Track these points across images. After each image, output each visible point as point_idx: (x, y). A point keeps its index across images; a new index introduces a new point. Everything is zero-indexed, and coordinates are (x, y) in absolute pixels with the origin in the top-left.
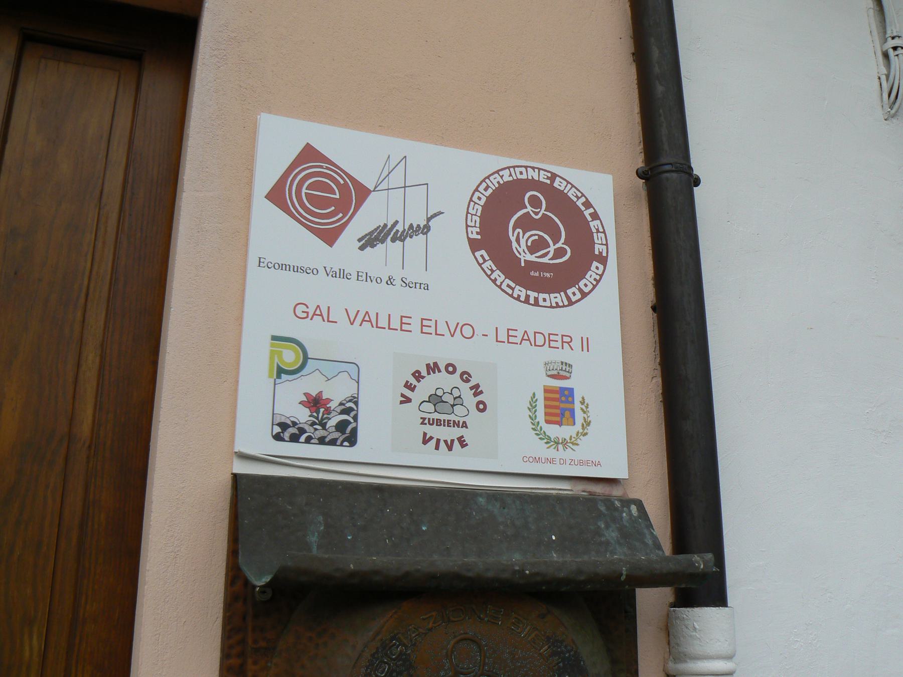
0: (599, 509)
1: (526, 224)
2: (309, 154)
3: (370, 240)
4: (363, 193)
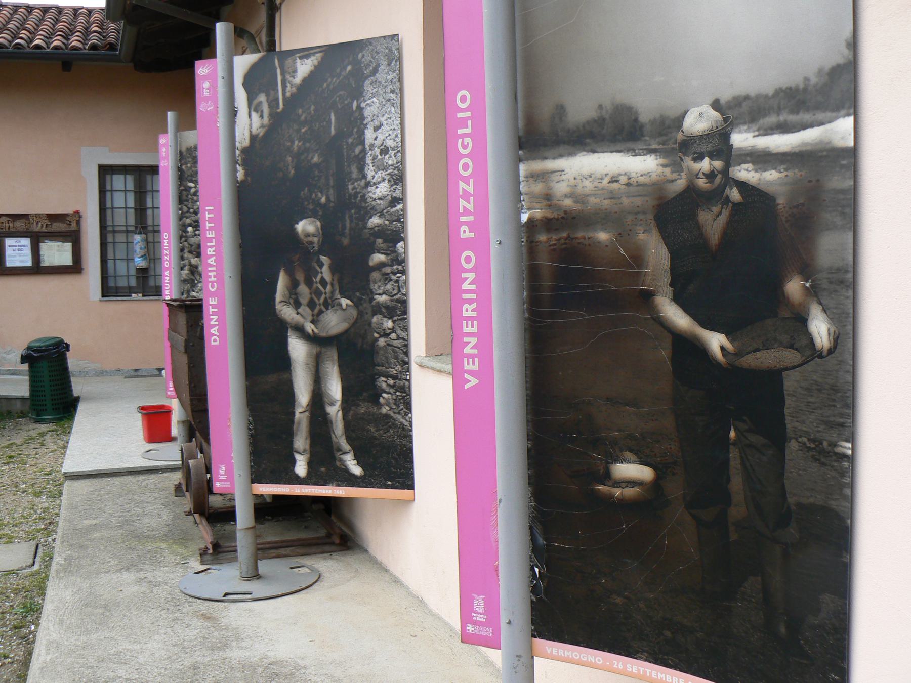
0: (305, 80)
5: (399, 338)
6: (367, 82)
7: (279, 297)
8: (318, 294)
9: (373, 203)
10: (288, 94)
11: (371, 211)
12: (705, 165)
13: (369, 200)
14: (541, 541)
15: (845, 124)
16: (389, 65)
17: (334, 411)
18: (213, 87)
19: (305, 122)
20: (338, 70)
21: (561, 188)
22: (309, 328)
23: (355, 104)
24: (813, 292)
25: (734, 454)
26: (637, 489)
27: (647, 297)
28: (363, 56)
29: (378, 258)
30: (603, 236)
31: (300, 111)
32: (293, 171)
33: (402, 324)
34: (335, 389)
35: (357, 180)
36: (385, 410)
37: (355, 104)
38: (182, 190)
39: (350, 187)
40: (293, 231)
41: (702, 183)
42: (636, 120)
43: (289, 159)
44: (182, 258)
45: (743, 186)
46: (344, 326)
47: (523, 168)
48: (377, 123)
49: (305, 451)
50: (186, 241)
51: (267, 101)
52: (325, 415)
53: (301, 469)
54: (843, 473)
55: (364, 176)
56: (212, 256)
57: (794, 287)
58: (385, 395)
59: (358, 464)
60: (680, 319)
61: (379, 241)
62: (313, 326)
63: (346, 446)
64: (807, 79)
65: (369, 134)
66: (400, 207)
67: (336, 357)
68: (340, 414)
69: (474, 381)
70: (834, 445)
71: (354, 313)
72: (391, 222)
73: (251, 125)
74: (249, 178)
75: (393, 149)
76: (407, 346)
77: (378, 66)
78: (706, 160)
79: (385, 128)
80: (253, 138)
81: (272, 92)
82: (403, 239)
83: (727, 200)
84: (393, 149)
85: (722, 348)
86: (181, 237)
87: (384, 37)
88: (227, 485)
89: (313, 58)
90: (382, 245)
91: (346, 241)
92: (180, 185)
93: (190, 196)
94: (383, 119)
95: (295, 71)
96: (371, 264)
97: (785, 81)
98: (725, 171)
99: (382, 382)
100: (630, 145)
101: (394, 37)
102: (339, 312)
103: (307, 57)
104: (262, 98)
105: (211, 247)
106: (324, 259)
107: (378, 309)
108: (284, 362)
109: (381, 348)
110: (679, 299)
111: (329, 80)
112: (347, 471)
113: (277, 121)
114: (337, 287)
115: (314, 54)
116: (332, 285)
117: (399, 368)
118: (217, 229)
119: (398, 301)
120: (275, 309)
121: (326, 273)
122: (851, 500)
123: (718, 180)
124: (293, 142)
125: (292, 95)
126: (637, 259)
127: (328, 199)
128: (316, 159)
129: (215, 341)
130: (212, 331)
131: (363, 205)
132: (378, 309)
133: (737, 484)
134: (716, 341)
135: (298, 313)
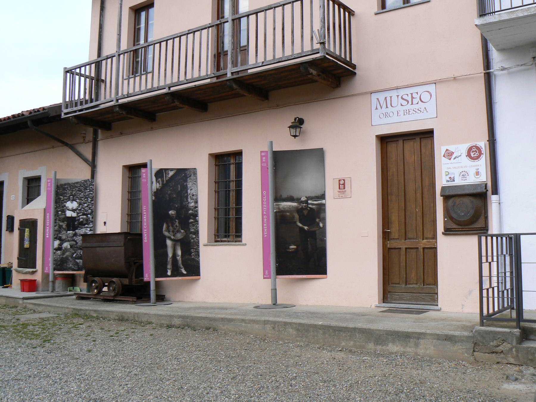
0: (171, 176)
1: (473, 152)
2: (447, 150)
3: (455, 159)
4: (453, 153)
5: (197, 240)
6: (188, 179)
7: (164, 230)
8: (175, 229)
9: (190, 207)
10: (167, 179)
11: (190, 209)
12: (304, 205)
13: (189, 207)
14: (278, 260)
15: (324, 201)
16: (194, 175)
17: (179, 258)
18: (147, 175)
19: (171, 187)
20: (180, 175)
21: (281, 207)
22: (172, 237)
23: (185, 183)
24: (320, 221)
25: (309, 243)
26: (294, 249)
27: (295, 222)
28: (187, 172)
29: (191, 220)
30: (288, 214)
31: (170, 184)
32: (168, 199)
33: (197, 236)
34: (179, 252)
35: (186, 202)
37: (185, 183)
38: (57, 199)
39: (184, 203)
40: (168, 214)
41: (304, 207)
42: (294, 198)
43: (167, 195)
44: (55, 223)
45: (310, 207)
46: (182, 237)
47: (275, 204)
48: (191, 189)
49: (170, 268)
50: (58, 217)
51: (161, 180)
53: (169, 273)
54: (325, 242)
55: (188, 201)
56: (145, 219)
57: (317, 220)
58: (193, 253)
59: (185, 271)
60: (300, 225)
61: (192, 216)
62: (173, 237)
63: (182, 266)
64: (319, 195)
65: (189, 191)
66: (197, 209)
67: (180, 244)
68: (181, 258)
69: (266, 236)
70: (323, 239)
71: (185, 234)
72: (195, 212)
73: (157, 186)
74: (156, 200)
75: (195, 195)
76: (199, 241)
77: (191, 175)
78: (304, 204)
80: (157, 189)
81: (163, 178)
82: (198, 216)
83: (308, 209)
84: (195, 195)
85: (307, 228)
86: (55, 215)
87: (193, 168)
88: (148, 279)
89: (174, 171)
90: (192, 218)
91: (183, 216)
92: (56, 197)
93: (60, 201)
94: (192, 188)
95: (169, 174)
96: (190, 222)
98: (307, 206)
99: (192, 250)
100: (293, 201)
101: (195, 169)
102: (181, 234)
103: (172, 171)
104: (160, 179)
105: (145, 216)
106: (177, 220)
107: (191, 233)
108: (165, 246)
109: (192, 242)
110: (300, 222)
111: (178, 177)
113: (164, 186)
114: (180, 227)
115: (174, 170)
116: (179, 227)
117: (197, 247)
118: (147, 212)
119: (196, 231)
120: (163, 233)
121: (177, 224)
122: (326, 245)
123: (306, 207)
124: (168, 191)
125: (168, 180)
126: (294, 217)
127: (178, 206)
128: (175, 196)
129: (146, 241)
130: (145, 238)
131: (187, 208)
132: (191, 233)
133: (309, 246)
134: (306, 228)
135: (169, 234)
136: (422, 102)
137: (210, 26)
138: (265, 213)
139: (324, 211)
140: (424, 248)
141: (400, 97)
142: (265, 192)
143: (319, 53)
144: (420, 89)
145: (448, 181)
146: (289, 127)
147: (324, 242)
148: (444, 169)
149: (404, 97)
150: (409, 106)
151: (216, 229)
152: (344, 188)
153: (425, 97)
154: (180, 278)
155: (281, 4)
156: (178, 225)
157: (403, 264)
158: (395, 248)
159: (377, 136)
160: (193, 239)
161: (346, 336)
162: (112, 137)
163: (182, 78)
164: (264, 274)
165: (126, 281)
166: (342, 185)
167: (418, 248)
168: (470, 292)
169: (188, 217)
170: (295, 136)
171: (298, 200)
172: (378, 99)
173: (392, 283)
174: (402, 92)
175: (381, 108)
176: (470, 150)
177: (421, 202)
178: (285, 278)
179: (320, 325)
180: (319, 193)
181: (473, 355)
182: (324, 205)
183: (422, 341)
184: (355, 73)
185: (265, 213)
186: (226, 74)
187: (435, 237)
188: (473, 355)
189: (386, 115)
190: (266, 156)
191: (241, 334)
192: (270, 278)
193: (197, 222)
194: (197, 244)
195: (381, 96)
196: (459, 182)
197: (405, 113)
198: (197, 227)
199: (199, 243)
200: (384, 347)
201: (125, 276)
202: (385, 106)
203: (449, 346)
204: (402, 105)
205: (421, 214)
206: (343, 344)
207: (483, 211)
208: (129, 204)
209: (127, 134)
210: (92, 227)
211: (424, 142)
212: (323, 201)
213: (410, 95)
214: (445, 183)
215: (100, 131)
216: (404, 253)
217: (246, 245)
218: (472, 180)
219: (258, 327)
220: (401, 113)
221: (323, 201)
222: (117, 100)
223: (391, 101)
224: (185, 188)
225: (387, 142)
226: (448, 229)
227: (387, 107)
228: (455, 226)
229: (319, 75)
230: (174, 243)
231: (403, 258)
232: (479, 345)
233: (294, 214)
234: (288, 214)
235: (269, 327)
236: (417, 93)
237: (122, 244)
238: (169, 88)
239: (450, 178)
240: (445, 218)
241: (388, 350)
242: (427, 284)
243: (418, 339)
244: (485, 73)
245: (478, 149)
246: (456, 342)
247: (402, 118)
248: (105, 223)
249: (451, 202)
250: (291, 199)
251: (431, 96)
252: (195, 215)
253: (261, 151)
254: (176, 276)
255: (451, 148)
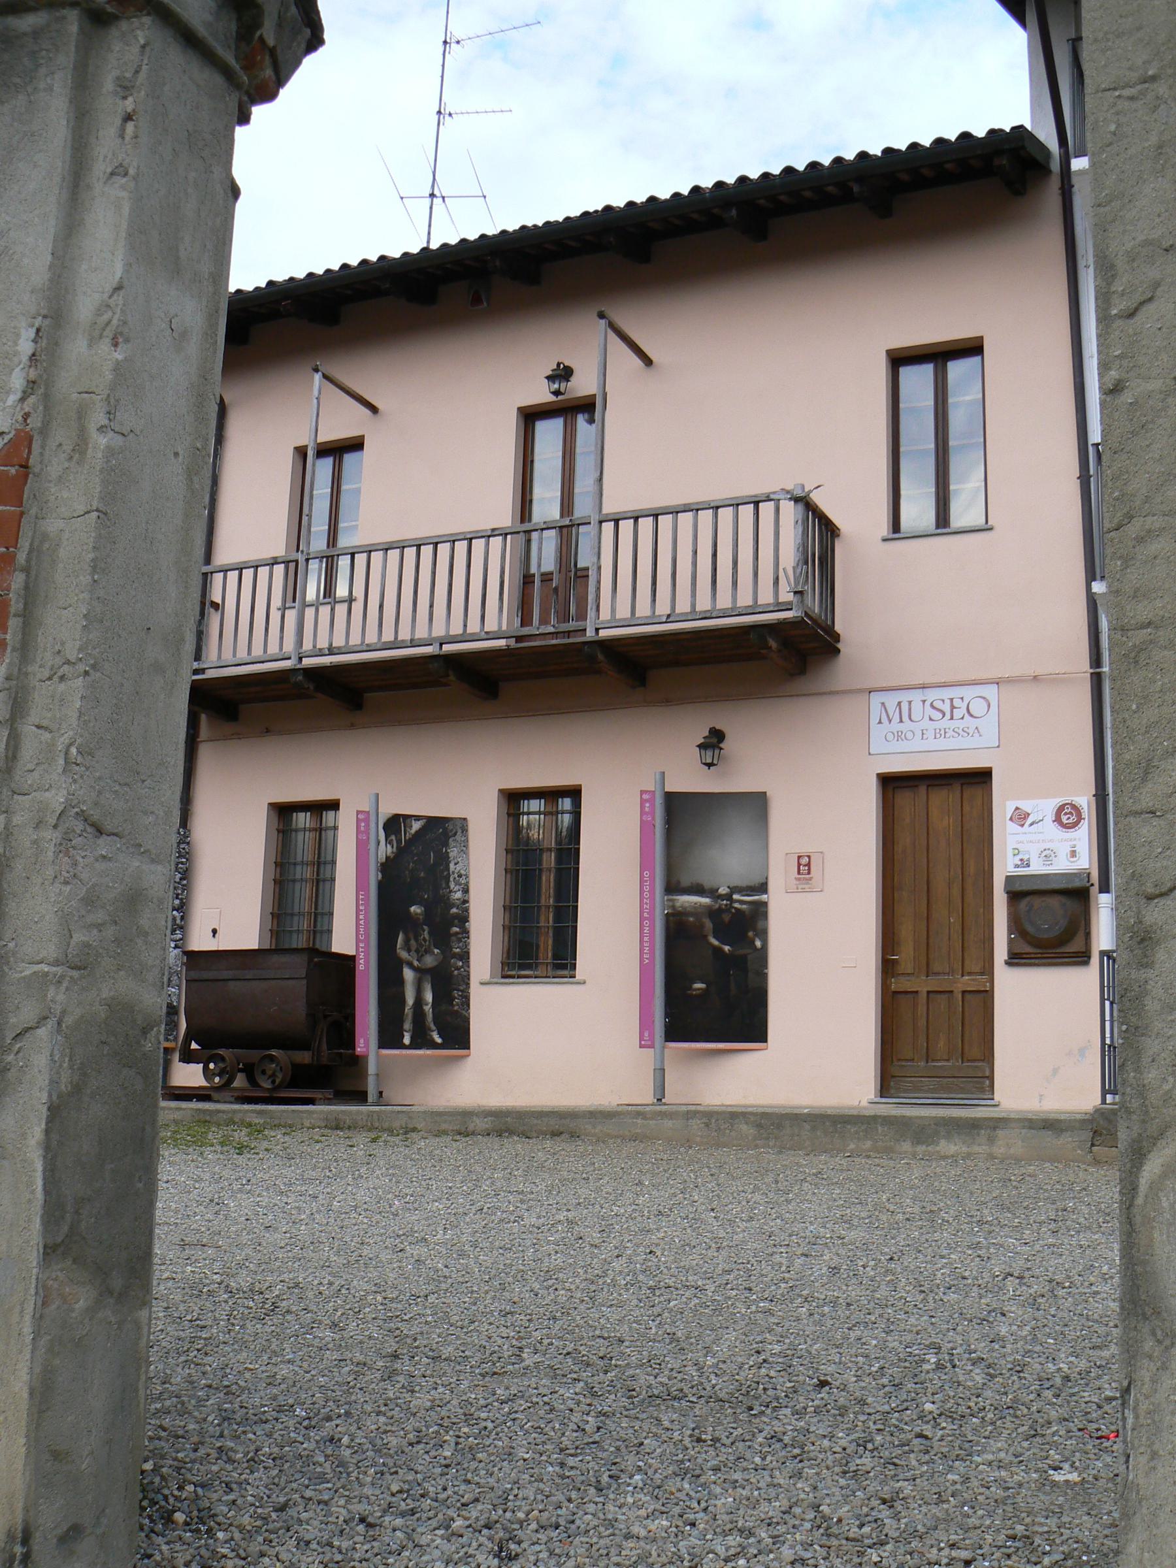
0: (416, 832)
1: (1066, 814)
2: (1017, 808)
3: (1031, 825)
4: (1029, 814)
6: (451, 840)
7: (398, 946)
8: (421, 946)
11: (453, 905)
12: (725, 902)
17: (428, 1009)
21: (678, 904)
22: (416, 963)
24: (756, 935)
27: (705, 937)
29: (456, 929)
30: (691, 919)
34: (429, 997)
36: (456, 1008)
40: (409, 911)
45: (735, 908)
46: (435, 964)
52: (423, 1011)
53: (407, 1040)
55: (449, 887)
57: (751, 934)
60: (715, 942)
63: (433, 1027)
65: (452, 866)
79: (460, 864)
80: (387, 858)
88: (364, 1050)
97: (749, 884)
99: (455, 993)
101: (465, 819)
104: (393, 837)
106: (425, 927)
107: (454, 956)
108: (401, 982)
110: (714, 937)
112: (433, 1041)
113: (401, 852)
121: (426, 936)
122: (767, 983)
126: (702, 926)
128: (422, 875)
134: (727, 948)
136: (971, 716)
137: (544, 526)
138: (646, 915)
139: (765, 915)
140: (964, 992)
141: (928, 704)
142: (647, 874)
143: (791, 609)
144: (968, 692)
145: (1017, 866)
146: (698, 746)
147: (763, 977)
148: (1011, 843)
149: (938, 704)
150: (946, 723)
151: (505, 950)
152: (809, 873)
153: (978, 707)
154: (429, 1052)
155: (712, 505)
156: (427, 936)
157: (922, 1022)
158: (906, 992)
159: (879, 775)
160: (458, 969)
161: (857, 1132)
162: (238, 736)
163: (474, 627)
164: (641, 1039)
165: (304, 1057)
166: (804, 866)
167: (952, 992)
168: (1082, 1051)
169: (450, 921)
170: (709, 765)
171: (712, 893)
172: (883, 704)
173: (899, 1060)
174: (932, 695)
175: (890, 721)
176: (1060, 810)
177: (960, 904)
178: (678, 1048)
179: (804, 1114)
180: (756, 880)
181: (1091, 1152)
182: (765, 904)
183: (1000, 1133)
184: (838, 651)
185: (646, 915)
186: (585, 630)
187: (988, 970)
188: (1091, 1152)
189: (899, 736)
190: (652, 801)
191: (635, 1141)
192: (652, 1046)
193: (466, 932)
194: (466, 979)
195: (891, 700)
196: (1037, 867)
197: (938, 736)
198: (467, 945)
199: (469, 979)
200: (930, 1148)
201: (304, 1046)
202: (896, 718)
203: (1049, 1139)
204: (931, 719)
205: (958, 927)
206: (852, 1146)
207: (1083, 922)
208: (277, 890)
209: (280, 733)
210: (181, 939)
211: (969, 792)
212: (764, 897)
213: (948, 702)
214: (1011, 870)
215: (203, 717)
216: (925, 1001)
217: (584, 983)
218: (1062, 865)
219: (673, 1124)
220: (930, 734)
221: (764, 897)
222: (300, 659)
223: (910, 709)
224: (444, 859)
225: (894, 788)
226: (1016, 954)
227: (901, 721)
228: (1029, 949)
229: (780, 651)
230: (418, 975)
231: (922, 1009)
232: (1101, 1135)
233: (704, 920)
234: (691, 919)
235: (696, 1124)
236: (962, 698)
237: (303, 973)
238: (441, 645)
239: (1021, 860)
240: (1010, 932)
241: (938, 1152)
242: (969, 1061)
243: (995, 1128)
244: (1092, 674)
245: (1076, 809)
246: (1062, 1131)
247: (931, 744)
248: (214, 932)
249: (1023, 904)
250: (698, 890)
251: (989, 706)
252: (463, 919)
253: (890, 783)
254: (420, 1048)
255: (1026, 806)
